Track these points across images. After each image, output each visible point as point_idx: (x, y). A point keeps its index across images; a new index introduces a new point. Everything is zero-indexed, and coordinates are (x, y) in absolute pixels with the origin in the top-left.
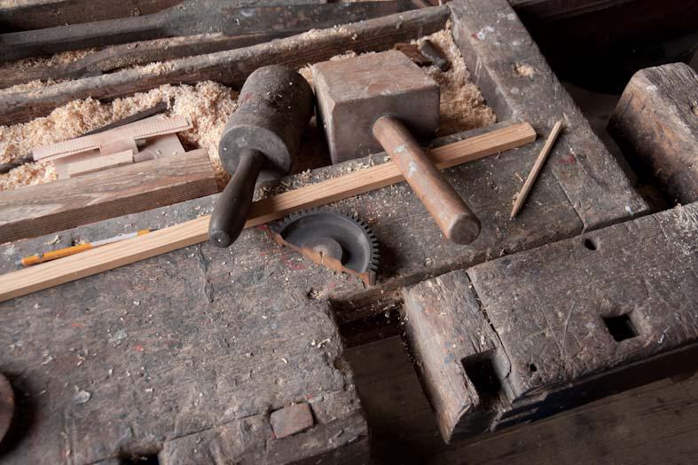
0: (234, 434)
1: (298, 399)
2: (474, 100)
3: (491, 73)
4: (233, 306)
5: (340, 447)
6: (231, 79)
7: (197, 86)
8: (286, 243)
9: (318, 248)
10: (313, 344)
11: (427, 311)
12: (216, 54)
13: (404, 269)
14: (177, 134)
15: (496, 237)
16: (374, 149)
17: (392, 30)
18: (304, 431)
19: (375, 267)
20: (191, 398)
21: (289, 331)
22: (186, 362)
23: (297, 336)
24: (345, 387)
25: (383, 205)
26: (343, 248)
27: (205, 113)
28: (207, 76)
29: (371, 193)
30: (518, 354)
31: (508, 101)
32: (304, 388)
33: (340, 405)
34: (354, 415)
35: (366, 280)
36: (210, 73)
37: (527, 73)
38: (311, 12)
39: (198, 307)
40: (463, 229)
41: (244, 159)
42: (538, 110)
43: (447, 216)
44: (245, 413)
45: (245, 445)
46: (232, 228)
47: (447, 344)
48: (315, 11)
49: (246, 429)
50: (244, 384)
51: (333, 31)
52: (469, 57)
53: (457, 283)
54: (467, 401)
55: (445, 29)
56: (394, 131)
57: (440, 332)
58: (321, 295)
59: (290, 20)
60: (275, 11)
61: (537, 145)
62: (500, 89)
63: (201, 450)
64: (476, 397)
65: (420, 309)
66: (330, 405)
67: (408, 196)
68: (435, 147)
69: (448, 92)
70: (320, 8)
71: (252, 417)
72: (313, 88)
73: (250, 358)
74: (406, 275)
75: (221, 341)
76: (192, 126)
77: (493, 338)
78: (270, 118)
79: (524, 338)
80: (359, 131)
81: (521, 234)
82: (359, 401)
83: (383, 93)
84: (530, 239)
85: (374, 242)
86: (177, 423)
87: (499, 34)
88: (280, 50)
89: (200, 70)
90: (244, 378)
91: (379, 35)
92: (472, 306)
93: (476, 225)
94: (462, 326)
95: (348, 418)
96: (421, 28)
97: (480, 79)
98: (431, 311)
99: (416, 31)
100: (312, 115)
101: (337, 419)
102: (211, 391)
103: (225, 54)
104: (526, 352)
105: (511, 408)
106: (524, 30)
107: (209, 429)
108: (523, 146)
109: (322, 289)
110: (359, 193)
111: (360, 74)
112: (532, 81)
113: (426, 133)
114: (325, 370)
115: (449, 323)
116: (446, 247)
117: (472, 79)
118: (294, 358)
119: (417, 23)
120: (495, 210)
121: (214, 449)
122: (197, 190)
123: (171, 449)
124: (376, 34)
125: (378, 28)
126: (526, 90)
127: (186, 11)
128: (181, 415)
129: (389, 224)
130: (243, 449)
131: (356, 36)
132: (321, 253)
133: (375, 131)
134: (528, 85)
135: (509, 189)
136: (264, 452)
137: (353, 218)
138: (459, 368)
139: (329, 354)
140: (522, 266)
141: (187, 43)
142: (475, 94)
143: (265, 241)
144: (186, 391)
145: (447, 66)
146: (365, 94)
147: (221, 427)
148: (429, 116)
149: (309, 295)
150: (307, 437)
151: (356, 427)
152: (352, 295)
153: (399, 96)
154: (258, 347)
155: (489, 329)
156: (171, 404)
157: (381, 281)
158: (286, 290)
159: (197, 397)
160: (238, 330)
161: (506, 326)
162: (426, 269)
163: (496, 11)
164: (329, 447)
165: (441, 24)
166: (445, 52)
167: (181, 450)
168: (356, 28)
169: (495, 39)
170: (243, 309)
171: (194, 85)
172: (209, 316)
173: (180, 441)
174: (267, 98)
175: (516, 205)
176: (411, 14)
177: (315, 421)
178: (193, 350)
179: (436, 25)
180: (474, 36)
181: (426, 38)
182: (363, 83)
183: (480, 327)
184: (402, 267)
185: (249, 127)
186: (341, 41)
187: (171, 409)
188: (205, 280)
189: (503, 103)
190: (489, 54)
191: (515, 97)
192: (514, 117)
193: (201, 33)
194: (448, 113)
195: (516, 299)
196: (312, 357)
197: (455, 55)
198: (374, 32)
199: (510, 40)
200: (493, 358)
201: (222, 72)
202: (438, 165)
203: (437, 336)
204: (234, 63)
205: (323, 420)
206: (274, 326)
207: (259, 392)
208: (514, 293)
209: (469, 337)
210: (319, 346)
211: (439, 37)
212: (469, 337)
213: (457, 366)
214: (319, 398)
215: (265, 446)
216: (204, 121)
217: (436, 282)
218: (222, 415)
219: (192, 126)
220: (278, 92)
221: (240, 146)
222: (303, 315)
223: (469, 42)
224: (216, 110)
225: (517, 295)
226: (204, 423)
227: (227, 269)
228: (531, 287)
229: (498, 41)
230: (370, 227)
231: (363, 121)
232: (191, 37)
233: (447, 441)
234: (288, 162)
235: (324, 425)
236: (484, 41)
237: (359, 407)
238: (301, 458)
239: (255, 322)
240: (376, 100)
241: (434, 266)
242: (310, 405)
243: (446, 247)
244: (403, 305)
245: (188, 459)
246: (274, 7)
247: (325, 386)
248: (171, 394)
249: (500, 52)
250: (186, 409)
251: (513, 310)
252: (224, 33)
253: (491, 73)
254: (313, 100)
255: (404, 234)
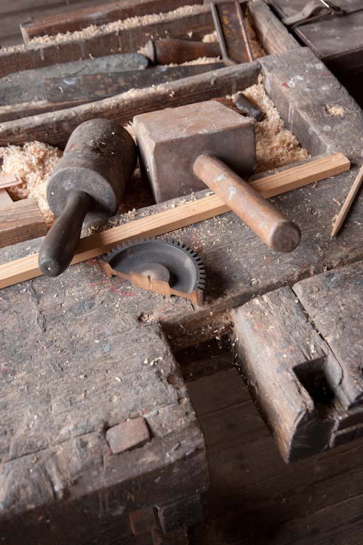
0: (70, 452)
1: (134, 414)
2: (289, 144)
3: (304, 115)
4: (66, 334)
5: (178, 461)
6: (56, 138)
7: (25, 146)
8: (115, 272)
9: (146, 273)
10: (146, 362)
11: (256, 327)
12: (41, 115)
13: (231, 290)
14: (7, 190)
15: (319, 256)
16: (198, 187)
17: (206, 86)
18: (140, 445)
19: (203, 286)
20: (25, 421)
21: (122, 352)
22: (20, 387)
23: (129, 357)
24: (179, 400)
25: (207, 235)
26: (168, 268)
27: (33, 170)
28: (34, 137)
29: (195, 225)
30: (348, 359)
31: (321, 137)
32: (139, 403)
33: (175, 418)
34: (189, 427)
35: (194, 300)
36: (37, 134)
37: (338, 113)
38: (131, 78)
39: (31, 337)
40: (283, 235)
41: (70, 201)
42: (351, 142)
43: (266, 225)
44: (81, 431)
45: (82, 462)
46: (61, 257)
47: (278, 355)
48: (134, 77)
49: (82, 447)
50: (79, 404)
51: (152, 90)
52: (282, 106)
53: (284, 299)
54: (302, 407)
55: (257, 84)
56: (214, 165)
57: (270, 345)
58: (151, 319)
59: (111, 86)
60: (96, 78)
61: (352, 173)
62: (313, 129)
63: (37, 470)
64: (310, 402)
65: (249, 326)
66: (166, 418)
67: (231, 225)
68: (253, 180)
69: (265, 139)
70: (139, 74)
71: (88, 435)
72: (134, 137)
73: (84, 380)
74: (233, 295)
75: (54, 366)
76: (20, 182)
77: (323, 346)
78: (95, 160)
79: (353, 343)
80: (181, 172)
81: (343, 251)
82: (194, 413)
83: (200, 132)
84: (352, 256)
85: (201, 269)
86: (11, 447)
87: (308, 81)
88: (102, 109)
89: (26, 130)
90: (78, 399)
91: (195, 91)
92: (299, 318)
93: (296, 232)
94: (291, 336)
95: (184, 429)
96: (235, 84)
97: (294, 124)
98: (260, 326)
99: (230, 87)
100: (134, 168)
101: (173, 432)
102: (46, 413)
103: (50, 115)
104: (356, 356)
105: (347, 416)
106: (332, 77)
107: (44, 449)
108: (338, 175)
109: (152, 313)
110: (183, 225)
111: (178, 120)
112: (343, 119)
113: (246, 171)
114: (159, 385)
115: (278, 335)
116: (270, 267)
117: (286, 127)
118: (128, 377)
119: (230, 79)
120: (316, 232)
121: (50, 468)
122: (29, 232)
123: (6, 471)
124: (192, 90)
125: (194, 85)
126: (338, 127)
127: (11, 82)
128: (16, 437)
129: (213, 251)
130: (79, 467)
131: (173, 93)
132: (149, 277)
133: (196, 168)
134: (339, 123)
135: (328, 213)
136: (101, 469)
137: (178, 244)
138: (291, 375)
139: (162, 371)
140: (346, 278)
141: (14, 111)
142: (290, 139)
143: (95, 274)
144: (20, 414)
145: (262, 117)
146: (184, 134)
147: (57, 446)
148: (244, 154)
149: (140, 319)
150: (144, 451)
151: (193, 439)
152: (182, 317)
153: (215, 134)
154: (92, 369)
155: (318, 338)
156: (6, 427)
157: (210, 302)
158: (117, 316)
159: (32, 419)
160: (71, 354)
161: (335, 333)
162: (252, 289)
163: (305, 63)
164: (167, 461)
165: (254, 79)
166: (259, 104)
167: (16, 471)
168: (173, 86)
169: (305, 86)
170: (76, 335)
171: (22, 146)
172: (42, 344)
173: (16, 462)
174: (91, 145)
175: (335, 226)
176: (224, 71)
177: (152, 435)
178: (26, 376)
179: (249, 80)
180: (285, 85)
181: (239, 92)
182: (181, 126)
183: (309, 337)
184: (228, 288)
185: (74, 169)
186: (159, 99)
187: (6, 433)
188: (37, 312)
189: (317, 141)
190: (300, 99)
191: (327, 133)
192: (328, 151)
193: (26, 101)
194: (266, 158)
195: (342, 308)
196: (145, 375)
197: (268, 105)
198: (190, 89)
199: (319, 86)
200: (325, 368)
201: (48, 132)
202: (262, 194)
203: (267, 347)
204: (59, 123)
205: (160, 434)
206: (107, 349)
207: (94, 411)
208: (340, 303)
209: (299, 347)
210: (152, 364)
211: (251, 91)
212: (299, 347)
213: (289, 374)
214: (153, 412)
215: (102, 462)
216: (32, 177)
217: (263, 300)
218: (58, 434)
219: (20, 182)
220: (102, 140)
221: (67, 189)
222: (135, 337)
223: (280, 91)
224: (44, 167)
225: (343, 305)
226: (39, 443)
227: (58, 301)
228: (356, 297)
229: (308, 87)
230: (197, 255)
231: (183, 160)
232: (17, 105)
233: (286, 461)
234: (114, 201)
235: (161, 439)
236: (294, 88)
237: (194, 419)
238: (140, 473)
239: (87, 346)
240: (192, 139)
241: (260, 285)
242: (145, 419)
243: (270, 267)
244: (233, 329)
245: (23, 478)
246: (96, 75)
247: (159, 400)
248: (7, 418)
249: (311, 96)
250: (21, 432)
251: (340, 319)
252: (49, 100)
253: (304, 115)
254: (136, 150)
255: (229, 259)
